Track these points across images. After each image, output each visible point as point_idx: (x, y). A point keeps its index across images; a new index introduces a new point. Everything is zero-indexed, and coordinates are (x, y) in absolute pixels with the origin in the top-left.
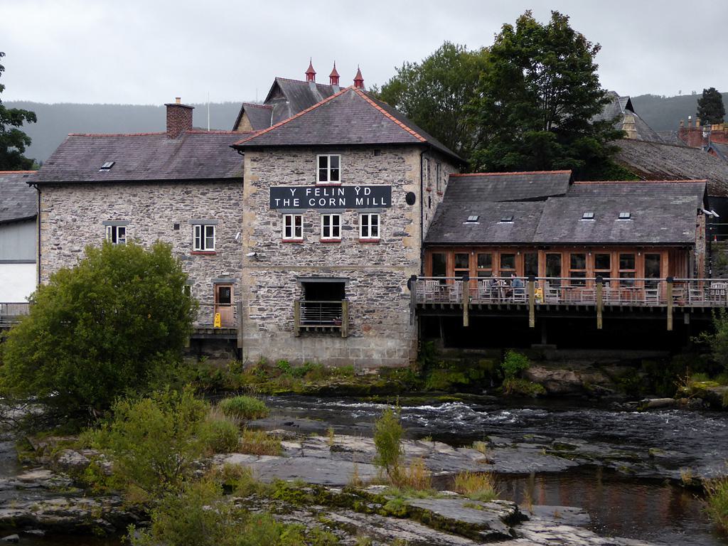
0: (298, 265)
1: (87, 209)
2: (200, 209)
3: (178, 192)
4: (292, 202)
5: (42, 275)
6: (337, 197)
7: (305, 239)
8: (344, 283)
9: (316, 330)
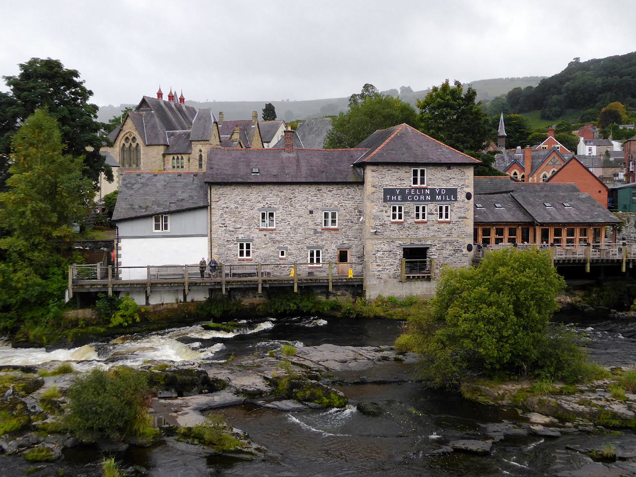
0: (401, 237)
1: (246, 200)
2: (327, 201)
3: (313, 188)
4: (397, 198)
5: (213, 244)
6: (425, 195)
7: (405, 221)
8: (428, 248)
9: (421, 277)
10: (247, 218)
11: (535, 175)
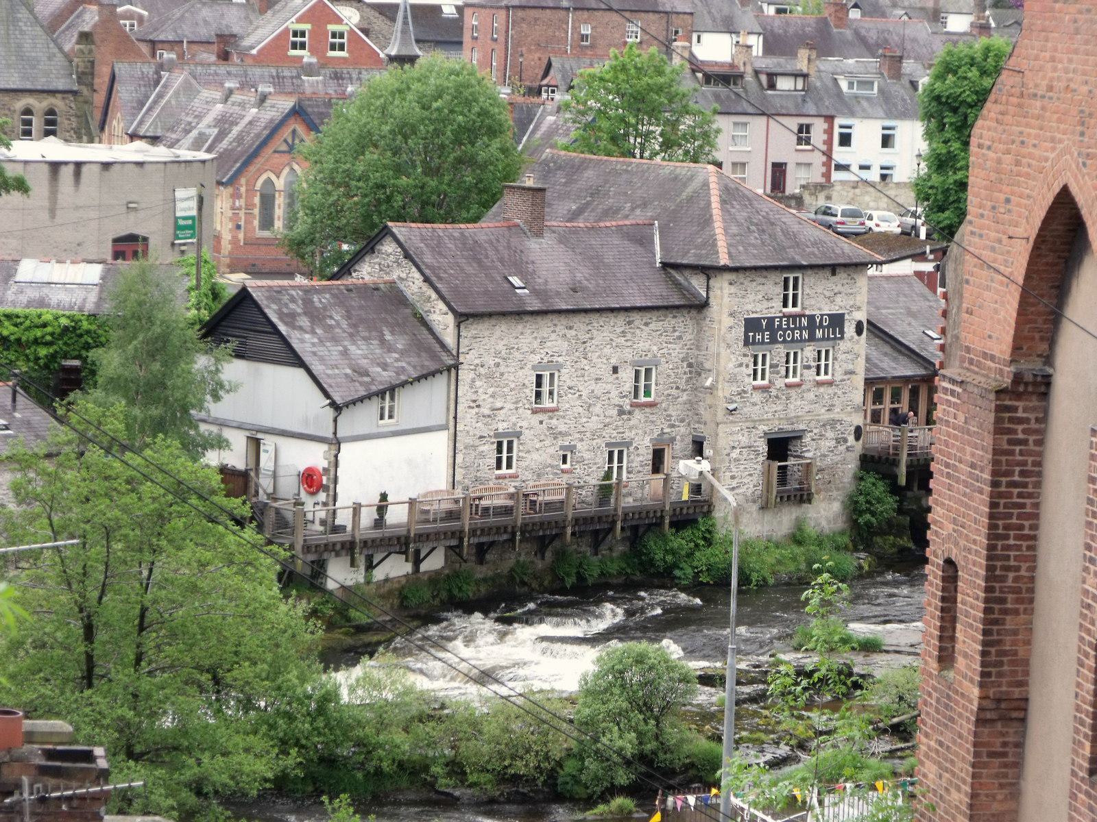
3: (619, 321)
6: (801, 329)
10: (513, 386)
11: (243, 181)
